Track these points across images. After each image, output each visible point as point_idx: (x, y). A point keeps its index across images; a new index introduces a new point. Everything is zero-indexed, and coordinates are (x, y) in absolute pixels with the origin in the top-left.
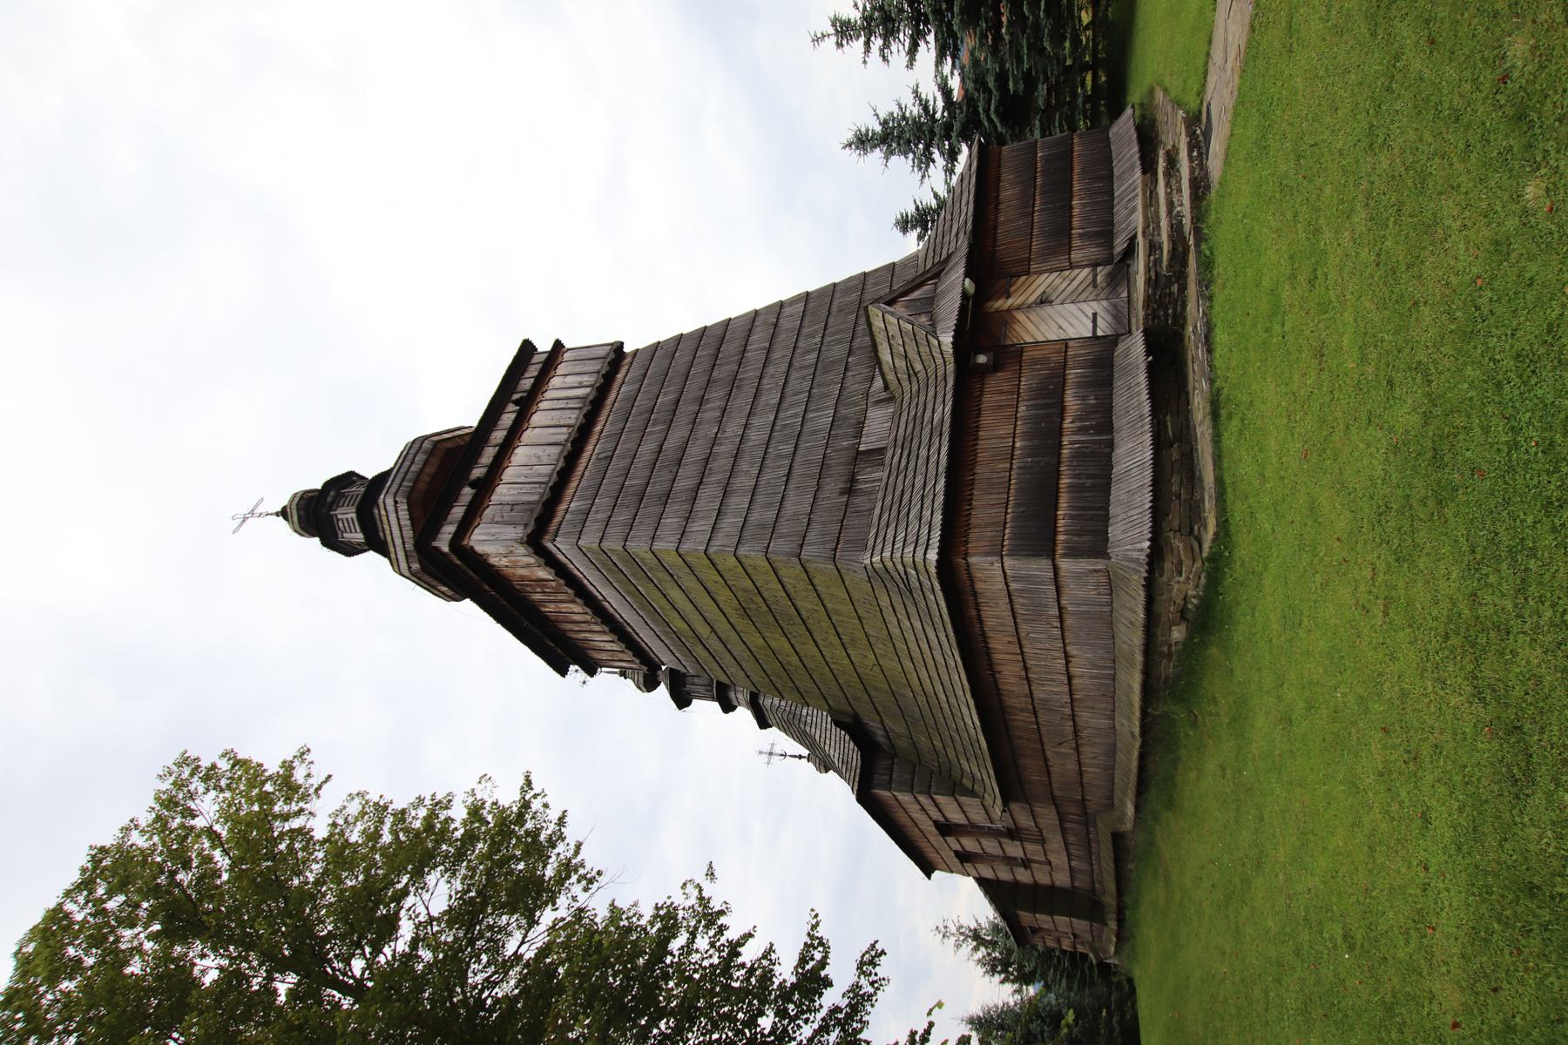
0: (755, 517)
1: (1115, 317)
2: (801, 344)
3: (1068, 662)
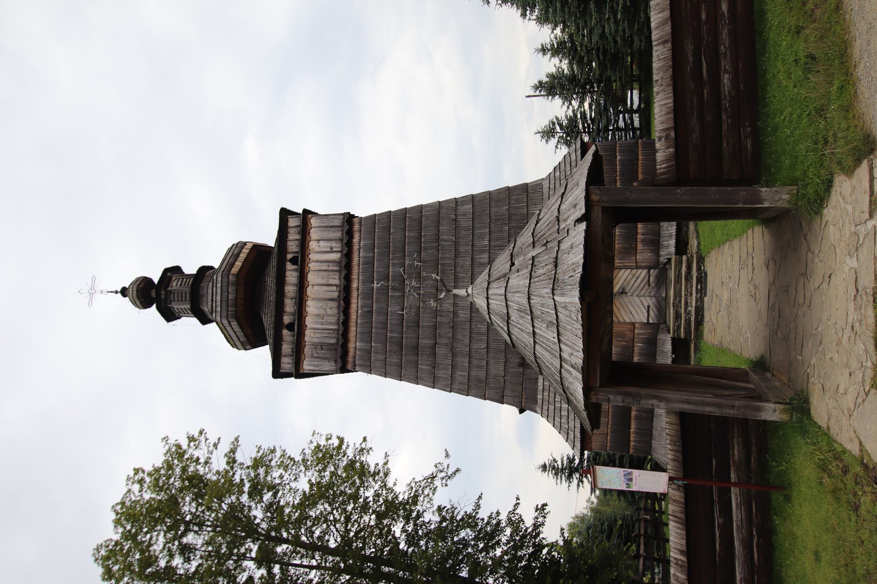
2: (477, 243)
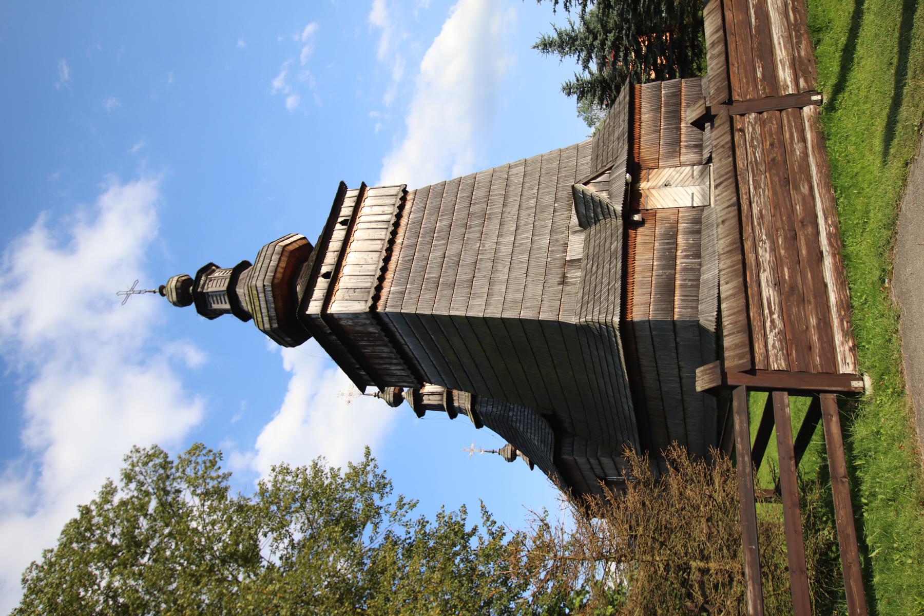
0: (510, 296)
1: (703, 196)
2: (525, 193)
3: (680, 370)
